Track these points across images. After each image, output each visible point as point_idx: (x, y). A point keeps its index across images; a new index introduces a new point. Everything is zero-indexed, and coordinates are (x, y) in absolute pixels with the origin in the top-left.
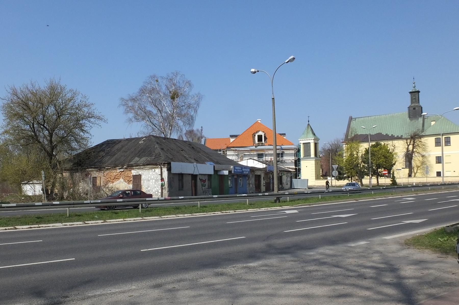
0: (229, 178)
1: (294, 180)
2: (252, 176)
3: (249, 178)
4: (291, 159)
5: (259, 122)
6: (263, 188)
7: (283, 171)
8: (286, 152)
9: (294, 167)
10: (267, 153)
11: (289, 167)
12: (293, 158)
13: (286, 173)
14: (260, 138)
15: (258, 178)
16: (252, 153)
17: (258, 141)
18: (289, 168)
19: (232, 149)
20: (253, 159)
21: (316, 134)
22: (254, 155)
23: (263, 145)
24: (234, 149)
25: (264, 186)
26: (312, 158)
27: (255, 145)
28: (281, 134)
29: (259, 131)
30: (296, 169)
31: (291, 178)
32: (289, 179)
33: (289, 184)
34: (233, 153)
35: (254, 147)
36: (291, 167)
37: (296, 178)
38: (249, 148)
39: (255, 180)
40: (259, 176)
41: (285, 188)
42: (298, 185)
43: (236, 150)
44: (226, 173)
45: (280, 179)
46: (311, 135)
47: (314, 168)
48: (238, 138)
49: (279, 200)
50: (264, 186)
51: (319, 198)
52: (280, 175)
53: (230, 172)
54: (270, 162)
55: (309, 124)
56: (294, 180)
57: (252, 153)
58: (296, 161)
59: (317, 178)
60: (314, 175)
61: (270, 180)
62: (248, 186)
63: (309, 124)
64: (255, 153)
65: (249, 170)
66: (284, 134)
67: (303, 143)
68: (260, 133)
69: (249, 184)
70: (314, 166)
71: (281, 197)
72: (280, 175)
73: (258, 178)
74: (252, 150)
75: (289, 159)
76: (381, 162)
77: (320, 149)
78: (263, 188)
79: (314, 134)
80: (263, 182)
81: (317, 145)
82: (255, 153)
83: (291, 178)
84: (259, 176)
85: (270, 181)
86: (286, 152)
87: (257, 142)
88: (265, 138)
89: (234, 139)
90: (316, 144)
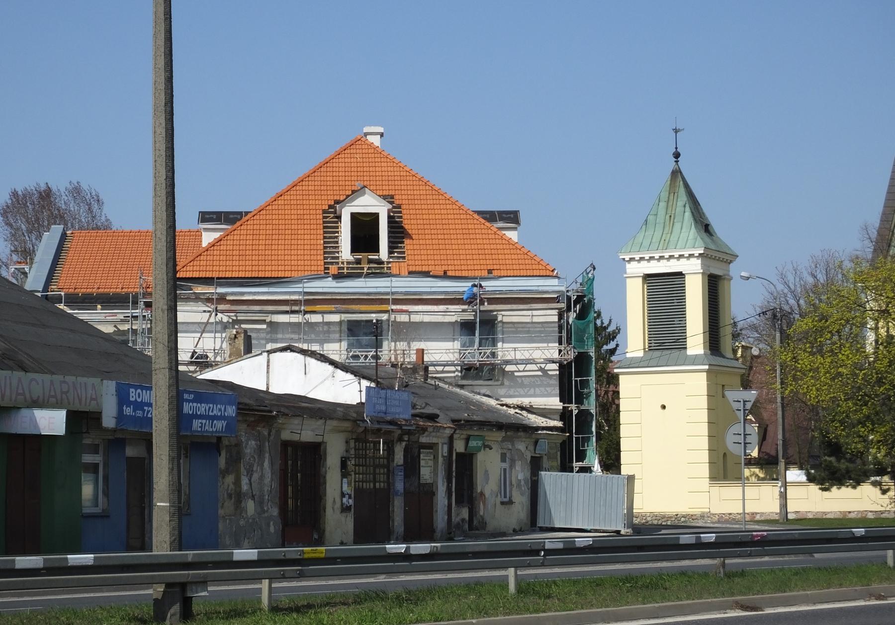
0: (87, 458)
1: (550, 479)
2: (260, 451)
3: (235, 459)
4: (537, 355)
5: (375, 140)
6: (338, 524)
7: (482, 424)
8: (507, 315)
9: (555, 403)
10: (403, 318)
11: (526, 401)
12: (548, 352)
13: (498, 435)
14: (364, 231)
15: (302, 465)
16: (316, 318)
17: (354, 249)
18: (530, 410)
19: (199, 289)
20: (303, 352)
21: (715, 226)
22: (324, 332)
23: (379, 271)
24: (210, 290)
25: (345, 509)
26: (695, 360)
27: (333, 270)
28: (490, 216)
29: (355, 193)
30: (565, 415)
31: (536, 465)
32: (521, 473)
33: (521, 500)
34: (204, 318)
35: (328, 285)
36: (539, 402)
37: (566, 467)
38: (298, 288)
39: (284, 477)
40: (313, 453)
41: (492, 525)
42: (576, 503)
43: (222, 299)
44: (51, 422)
45: (463, 469)
46: (687, 230)
47: (704, 416)
48: (243, 230)
49: (187, 603)
50: (345, 509)
51: (504, 585)
52: (459, 446)
53: (81, 420)
54: (415, 370)
55: (676, 173)
56: (550, 479)
57: (316, 318)
58: (564, 368)
59: (723, 469)
60: (705, 456)
61: (390, 473)
62: (229, 506)
63: (676, 173)
64: (336, 318)
65: (231, 411)
66: (512, 218)
67: (647, 277)
68: (368, 203)
69: (238, 497)
70: (703, 402)
71: (203, 583)
72: (459, 446)
73: (302, 465)
74: (313, 302)
75: (532, 353)
76: (126, 342)
77: (744, 304)
78: (338, 524)
79: (706, 228)
80: (336, 487)
81: (723, 286)
82: (336, 318)
83: (536, 465)
84: (313, 453)
85: (390, 484)
86: (507, 315)
87: (345, 252)
88: (398, 233)
89: (217, 235)
90: (714, 286)
